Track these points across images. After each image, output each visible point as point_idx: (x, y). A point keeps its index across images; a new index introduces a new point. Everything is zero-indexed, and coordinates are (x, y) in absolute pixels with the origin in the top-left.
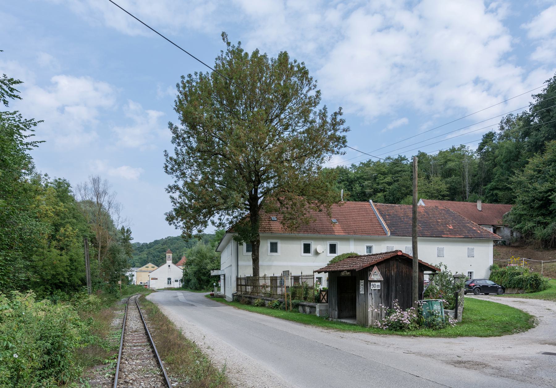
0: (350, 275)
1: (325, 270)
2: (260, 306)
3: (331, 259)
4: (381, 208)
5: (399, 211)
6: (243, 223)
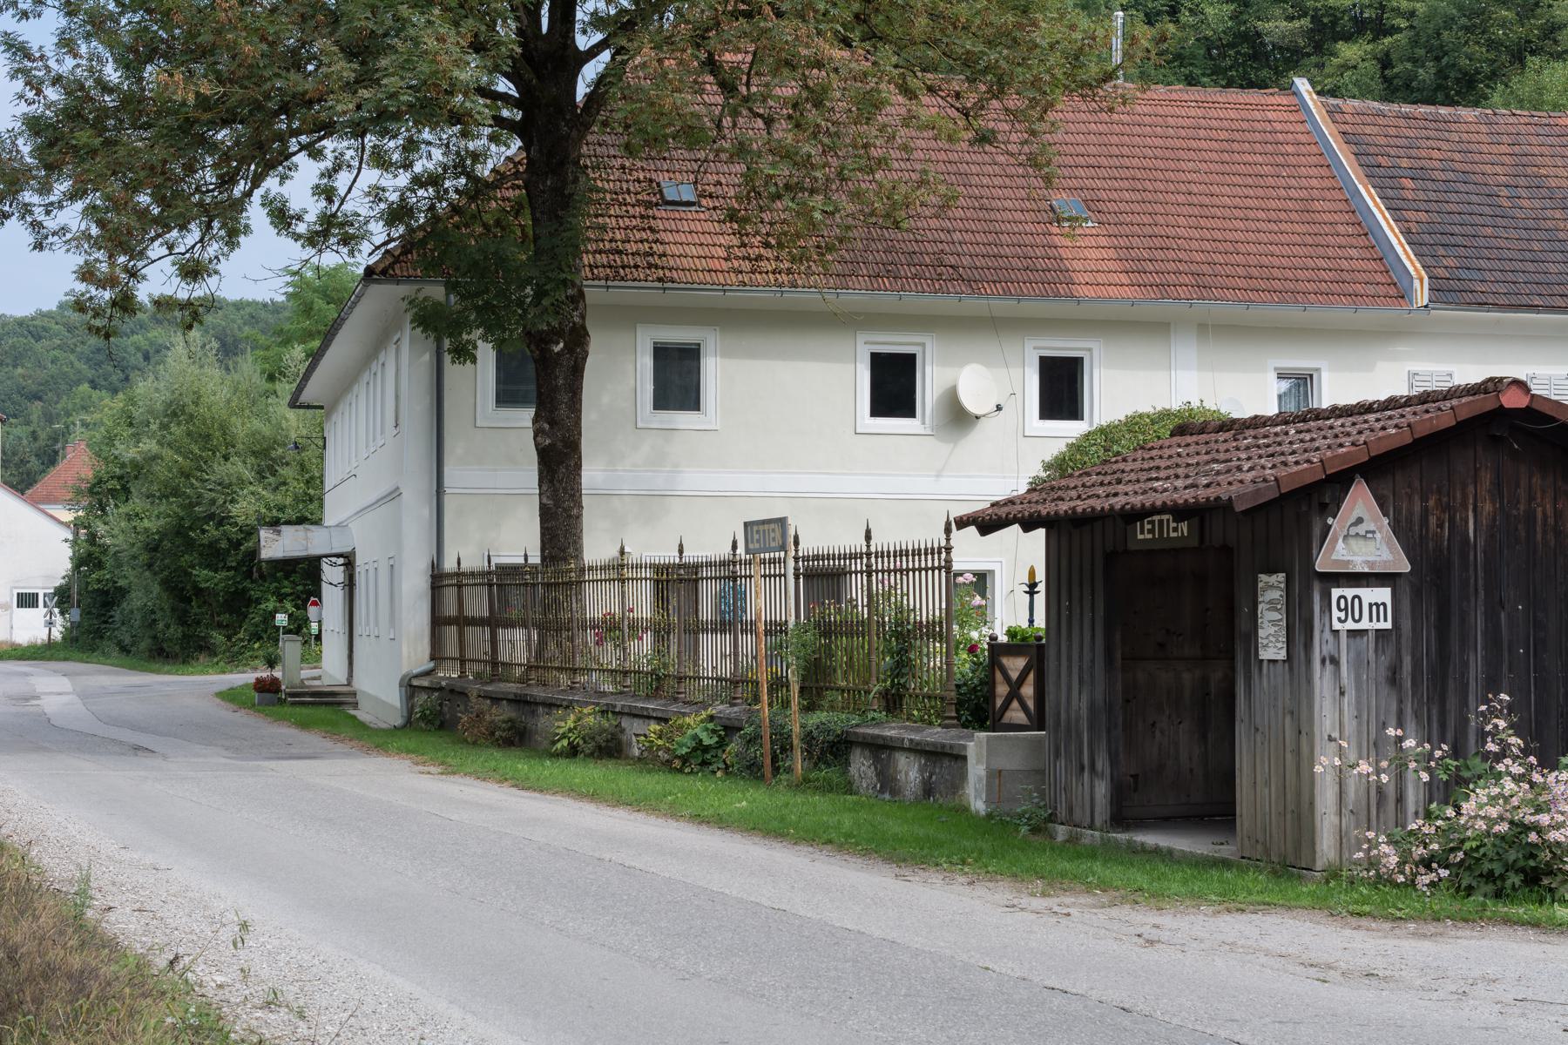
0: (1195, 543)
1: (1028, 510)
2: (591, 755)
3: (1055, 449)
4: (1368, 130)
5: (1484, 148)
6: (476, 217)
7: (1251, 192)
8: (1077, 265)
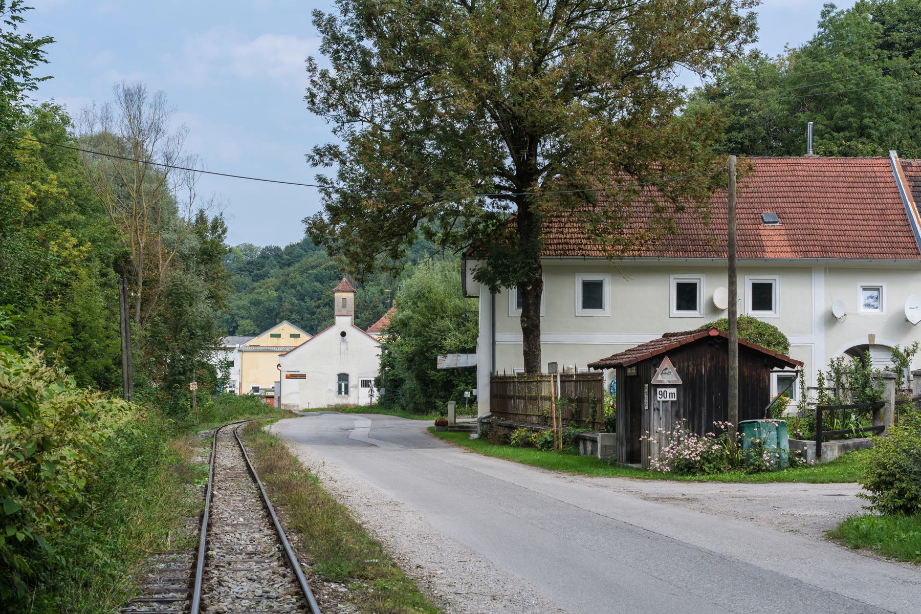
0: (636, 374)
7: (858, 207)
8: (768, 243)
